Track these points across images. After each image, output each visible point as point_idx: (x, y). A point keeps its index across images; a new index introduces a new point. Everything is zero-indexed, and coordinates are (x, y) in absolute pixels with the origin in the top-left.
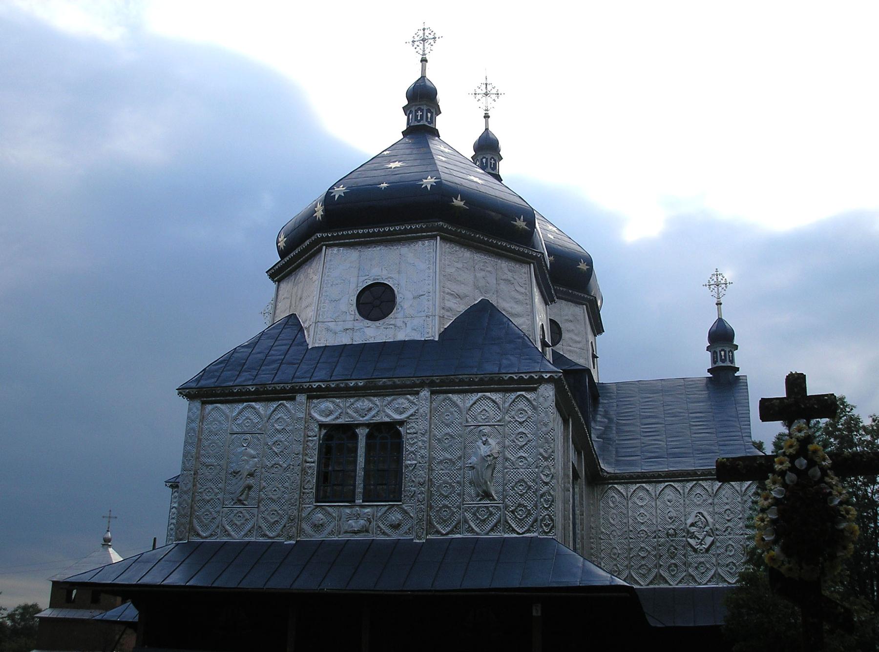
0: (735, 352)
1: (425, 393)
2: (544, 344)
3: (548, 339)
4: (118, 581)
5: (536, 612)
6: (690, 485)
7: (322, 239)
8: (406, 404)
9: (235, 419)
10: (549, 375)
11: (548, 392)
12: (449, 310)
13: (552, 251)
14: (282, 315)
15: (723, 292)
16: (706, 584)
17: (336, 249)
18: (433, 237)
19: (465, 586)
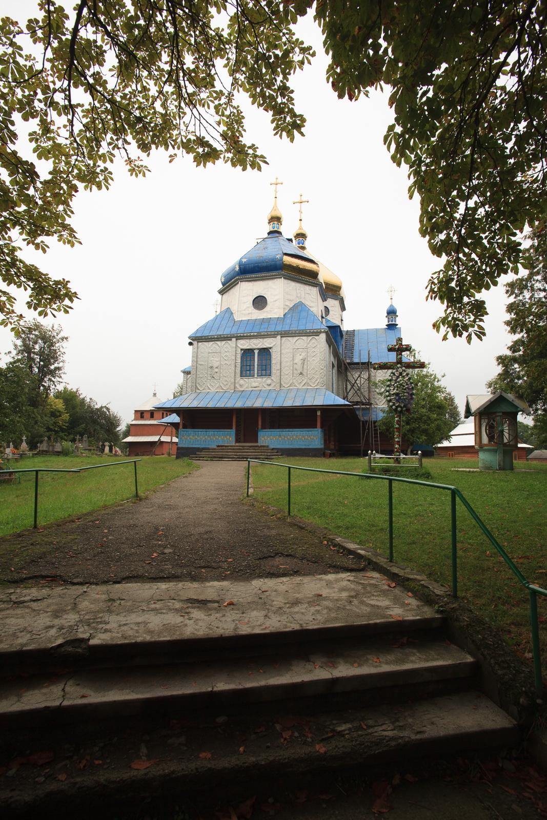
1: (279, 337)
2: (322, 317)
3: (324, 315)
4: (173, 406)
5: (319, 413)
7: (238, 279)
8: (272, 341)
11: (323, 337)
13: (326, 284)
14: (224, 308)
18: (281, 278)
19: (294, 405)
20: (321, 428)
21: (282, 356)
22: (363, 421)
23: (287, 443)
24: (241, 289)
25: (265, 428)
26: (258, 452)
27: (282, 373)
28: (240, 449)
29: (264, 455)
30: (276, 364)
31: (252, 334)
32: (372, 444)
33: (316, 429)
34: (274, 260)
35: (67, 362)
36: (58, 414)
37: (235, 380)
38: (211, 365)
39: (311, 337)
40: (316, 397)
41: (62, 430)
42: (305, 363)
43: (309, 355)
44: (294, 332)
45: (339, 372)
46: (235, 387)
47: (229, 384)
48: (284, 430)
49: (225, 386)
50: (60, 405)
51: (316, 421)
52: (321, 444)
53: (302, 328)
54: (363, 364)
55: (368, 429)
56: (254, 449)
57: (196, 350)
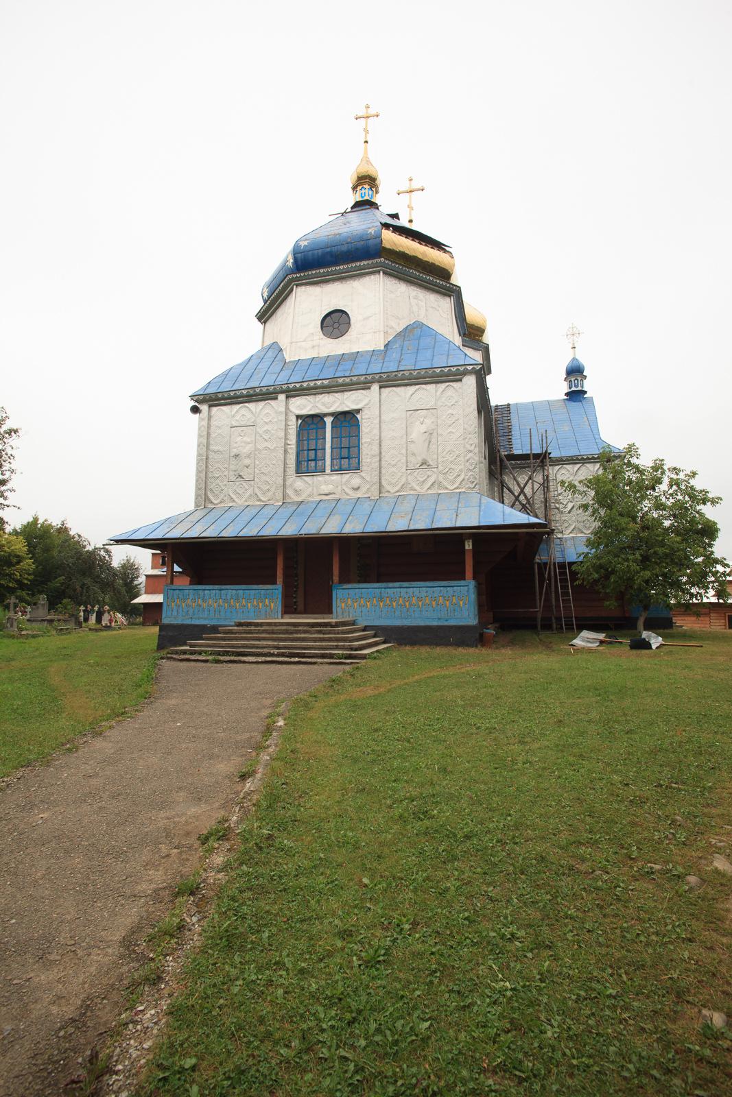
0: (584, 381)
1: (375, 387)
5: (469, 546)
6: (558, 467)
9: (234, 416)
10: (471, 367)
12: (392, 328)
14: (268, 342)
15: (577, 339)
16: (568, 534)
17: (303, 287)
19: (412, 527)
20: (474, 578)
21: (383, 426)
22: (539, 564)
23: (398, 613)
24: (298, 299)
25: (349, 582)
26: (330, 640)
27: (383, 463)
28: (286, 632)
29: (343, 648)
30: (370, 443)
31: (319, 383)
32: (558, 606)
33: (462, 583)
34: (363, 238)
35: (18, 472)
36: (15, 560)
37: (284, 480)
38: (235, 451)
39: (443, 386)
40: (461, 510)
41: (21, 586)
42: (434, 440)
43: (439, 422)
44: (407, 373)
45: (491, 474)
46: (285, 495)
47: (273, 489)
48: (391, 585)
49: (264, 493)
50: (20, 546)
51: (463, 563)
52: (472, 615)
53: (424, 364)
54: (536, 456)
55: (549, 579)
56: (320, 632)
57: (205, 423)
